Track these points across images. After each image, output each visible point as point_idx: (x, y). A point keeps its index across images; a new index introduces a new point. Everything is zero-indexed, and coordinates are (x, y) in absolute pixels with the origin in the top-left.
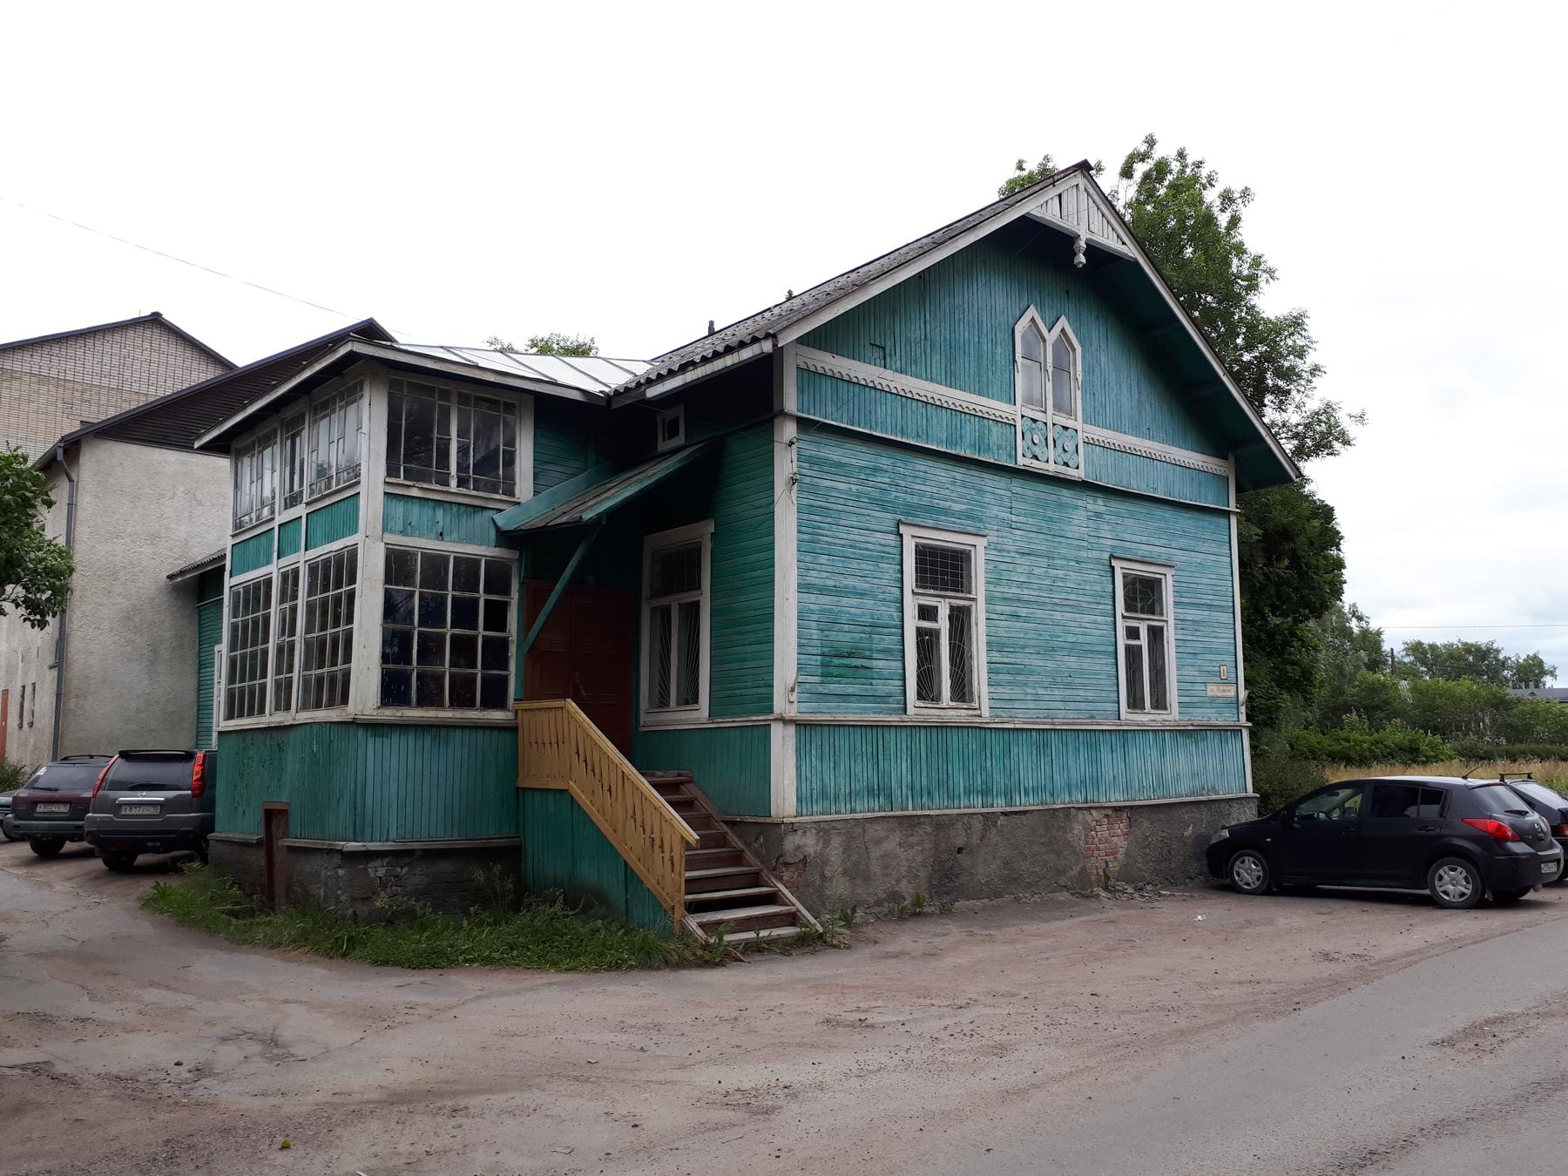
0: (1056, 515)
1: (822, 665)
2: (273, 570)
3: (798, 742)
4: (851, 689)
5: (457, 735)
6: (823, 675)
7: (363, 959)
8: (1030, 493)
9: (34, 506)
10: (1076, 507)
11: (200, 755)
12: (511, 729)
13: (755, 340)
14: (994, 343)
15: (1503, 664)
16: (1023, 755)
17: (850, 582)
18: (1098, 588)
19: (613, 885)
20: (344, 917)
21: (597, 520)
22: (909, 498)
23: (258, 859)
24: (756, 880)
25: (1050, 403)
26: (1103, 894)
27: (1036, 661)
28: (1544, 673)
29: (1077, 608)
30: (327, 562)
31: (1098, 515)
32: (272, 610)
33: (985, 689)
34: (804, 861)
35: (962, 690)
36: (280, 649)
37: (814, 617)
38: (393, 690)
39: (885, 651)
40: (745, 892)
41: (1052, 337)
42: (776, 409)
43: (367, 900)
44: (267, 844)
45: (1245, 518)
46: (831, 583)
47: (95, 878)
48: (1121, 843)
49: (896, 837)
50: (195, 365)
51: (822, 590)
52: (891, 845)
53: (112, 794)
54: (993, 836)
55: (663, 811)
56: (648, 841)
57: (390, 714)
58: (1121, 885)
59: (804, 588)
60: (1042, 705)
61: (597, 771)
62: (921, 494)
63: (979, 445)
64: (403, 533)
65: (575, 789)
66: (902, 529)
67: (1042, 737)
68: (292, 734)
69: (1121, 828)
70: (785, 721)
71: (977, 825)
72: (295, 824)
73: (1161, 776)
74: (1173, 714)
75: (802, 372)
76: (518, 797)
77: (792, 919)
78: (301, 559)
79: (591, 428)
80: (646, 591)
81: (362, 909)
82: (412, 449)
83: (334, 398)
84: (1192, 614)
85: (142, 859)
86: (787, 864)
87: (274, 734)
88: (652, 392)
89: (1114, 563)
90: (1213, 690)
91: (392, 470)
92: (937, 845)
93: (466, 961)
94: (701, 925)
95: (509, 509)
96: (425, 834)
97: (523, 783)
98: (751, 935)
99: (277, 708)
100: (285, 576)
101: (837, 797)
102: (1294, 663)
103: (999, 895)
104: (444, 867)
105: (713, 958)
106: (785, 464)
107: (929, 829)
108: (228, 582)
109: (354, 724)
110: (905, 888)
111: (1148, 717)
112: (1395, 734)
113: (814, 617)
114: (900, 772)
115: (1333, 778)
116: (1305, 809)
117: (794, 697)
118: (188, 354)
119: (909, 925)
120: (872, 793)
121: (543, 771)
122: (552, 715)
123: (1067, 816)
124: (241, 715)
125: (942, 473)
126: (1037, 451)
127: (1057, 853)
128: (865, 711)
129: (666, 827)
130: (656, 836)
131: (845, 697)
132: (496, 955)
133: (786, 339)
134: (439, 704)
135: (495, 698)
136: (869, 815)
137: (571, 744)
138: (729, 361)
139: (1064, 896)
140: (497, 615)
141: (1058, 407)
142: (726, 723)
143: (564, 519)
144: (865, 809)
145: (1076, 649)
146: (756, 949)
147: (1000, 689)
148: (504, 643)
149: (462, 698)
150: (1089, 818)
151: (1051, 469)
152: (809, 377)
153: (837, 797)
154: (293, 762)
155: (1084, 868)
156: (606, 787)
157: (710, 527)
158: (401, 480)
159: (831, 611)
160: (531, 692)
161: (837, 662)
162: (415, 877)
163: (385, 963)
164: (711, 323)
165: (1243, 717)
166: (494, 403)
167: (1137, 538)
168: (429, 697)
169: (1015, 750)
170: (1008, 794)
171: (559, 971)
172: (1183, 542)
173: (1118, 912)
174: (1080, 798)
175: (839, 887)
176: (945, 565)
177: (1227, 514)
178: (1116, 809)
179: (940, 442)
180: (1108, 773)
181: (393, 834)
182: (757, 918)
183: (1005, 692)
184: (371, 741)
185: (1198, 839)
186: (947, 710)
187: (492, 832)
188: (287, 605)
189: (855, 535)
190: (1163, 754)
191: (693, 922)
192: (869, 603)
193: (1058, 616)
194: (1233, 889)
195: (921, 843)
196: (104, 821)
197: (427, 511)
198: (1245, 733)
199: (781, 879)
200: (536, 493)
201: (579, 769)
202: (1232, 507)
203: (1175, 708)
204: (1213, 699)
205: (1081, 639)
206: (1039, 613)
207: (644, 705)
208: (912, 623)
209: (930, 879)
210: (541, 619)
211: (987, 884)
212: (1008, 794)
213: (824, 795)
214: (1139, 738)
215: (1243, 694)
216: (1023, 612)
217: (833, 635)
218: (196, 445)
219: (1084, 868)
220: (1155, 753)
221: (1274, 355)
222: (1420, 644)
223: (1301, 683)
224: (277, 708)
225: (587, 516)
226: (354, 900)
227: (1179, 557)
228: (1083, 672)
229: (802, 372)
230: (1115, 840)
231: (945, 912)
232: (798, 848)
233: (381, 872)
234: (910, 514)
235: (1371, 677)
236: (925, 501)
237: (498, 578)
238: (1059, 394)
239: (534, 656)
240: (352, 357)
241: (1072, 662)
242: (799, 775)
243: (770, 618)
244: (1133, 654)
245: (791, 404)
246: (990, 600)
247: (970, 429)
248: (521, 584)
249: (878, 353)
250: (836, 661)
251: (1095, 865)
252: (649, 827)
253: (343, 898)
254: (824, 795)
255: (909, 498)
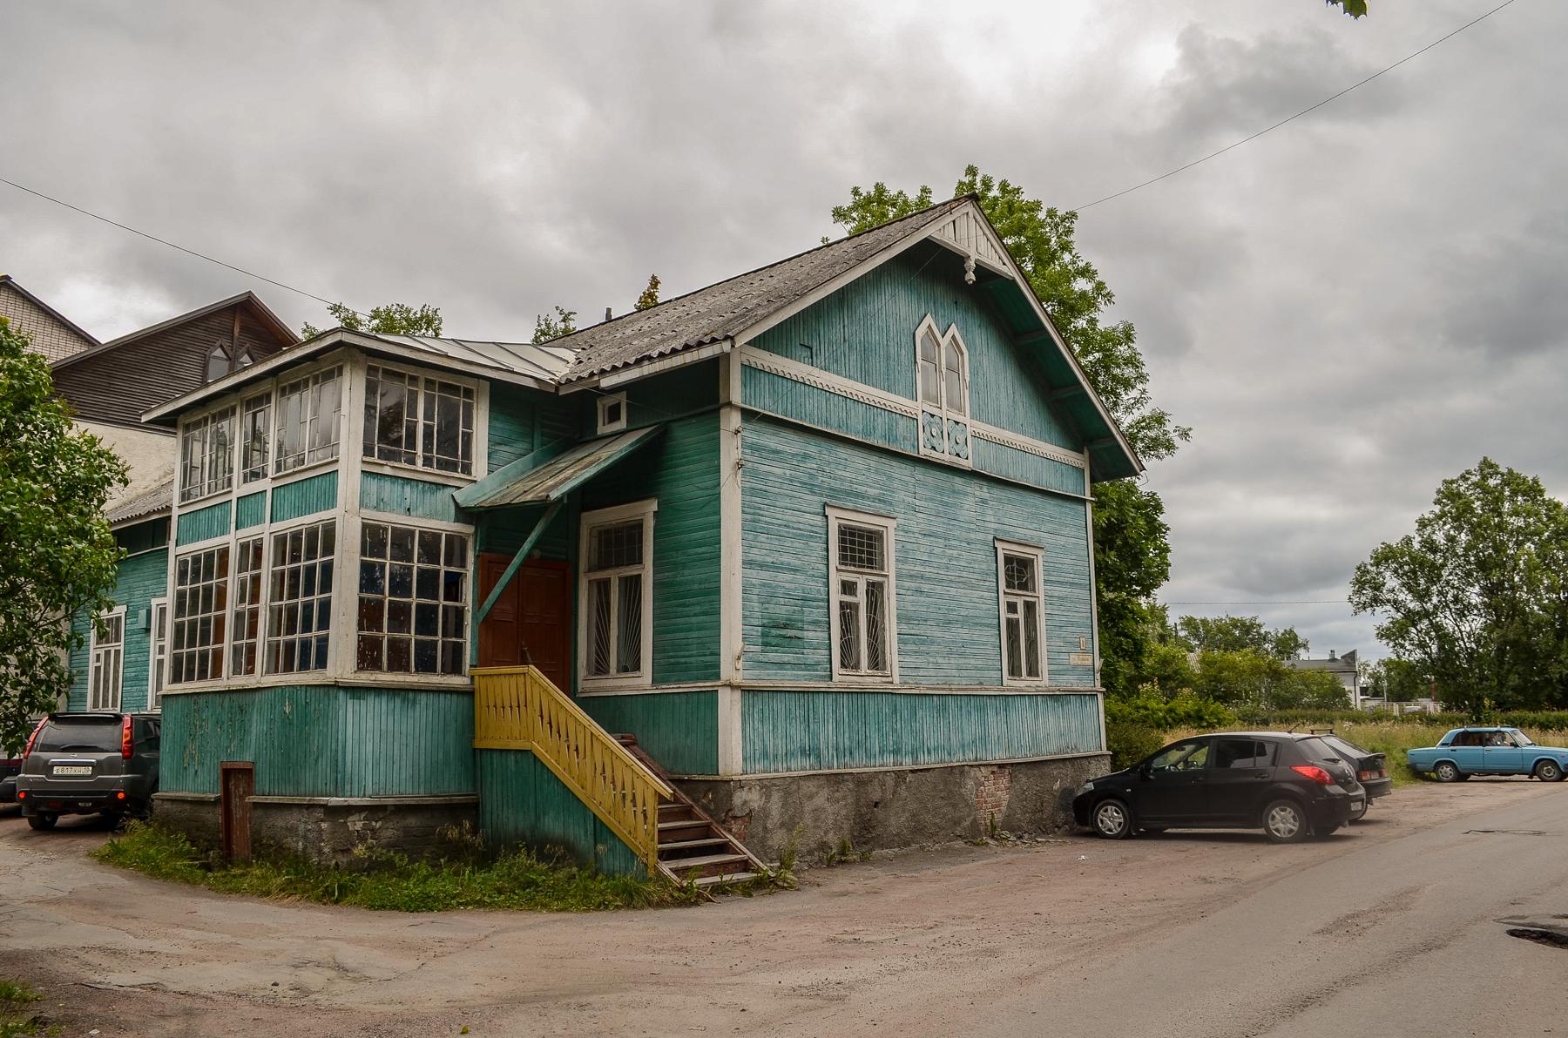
0: (951, 500)
1: (764, 635)
2: (232, 540)
3: (743, 706)
4: (787, 658)
5: (423, 698)
6: (765, 644)
7: (358, 904)
8: (929, 480)
9: (110, 485)
10: (966, 494)
11: (127, 719)
12: (469, 694)
13: (714, 341)
14: (899, 346)
15: (1265, 638)
16: (925, 716)
17: (785, 559)
18: (984, 566)
19: (581, 836)
20: (328, 867)
21: (560, 500)
22: (832, 482)
23: (215, 817)
24: (707, 831)
25: (944, 400)
26: (991, 842)
27: (936, 633)
28: (1298, 646)
29: (967, 584)
30: (296, 537)
31: (984, 501)
32: (230, 579)
33: (896, 658)
34: (749, 815)
35: (877, 661)
36: (239, 616)
37: (756, 591)
38: (368, 656)
39: (814, 623)
40: (707, 843)
41: (945, 342)
42: (722, 401)
43: (347, 851)
44: (225, 801)
45: (1100, 506)
46: (769, 560)
47: (23, 837)
48: (1004, 797)
49: (825, 793)
50: (40, 329)
51: (762, 566)
52: (820, 800)
53: (45, 755)
54: (903, 792)
55: (635, 768)
56: (619, 797)
57: (367, 678)
58: (1006, 833)
59: (748, 564)
60: (941, 673)
61: (563, 732)
62: (842, 479)
63: (890, 434)
64: (377, 508)
65: (539, 750)
66: (828, 511)
67: (941, 700)
68: (258, 696)
69: (1004, 782)
70: (732, 687)
71: (890, 782)
72: (263, 780)
73: (1034, 737)
74: (1044, 681)
75: (747, 368)
76: (475, 759)
77: (745, 866)
78: (265, 531)
79: (546, 416)
80: (583, 566)
81: (343, 859)
82: (387, 434)
83: (306, 382)
84: (1059, 591)
85: (62, 820)
86: (735, 818)
87: (234, 697)
88: (605, 383)
89: (997, 544)
90: (1074, 659)
91: (368, 451)
92: (858, 800)
93: (460, 904)
94: (675, 871)
95: (467, 487)
96: (396, 789)
97: (479, 744)
98: (717, 879)
99: (236, 671)
100: (244, 547)
101: (775, 756)
102: (1127, 636)
103: (907, 844)
104: (412, 821)
105: (688, 899)
106: (730, 451)
107: (851, 786)
108: (173, 550)
109: (336, 686)
110: (833, 839)
111: (1024, 683)
112: (1186, 701)
113: (756, 591)
114: (827, 734)
115: (1168, 740)
116: (1158, 763)
117: (739, 666)
118: (34, 316)
119: (839, 871)
120: (803, 752)
121: (501, 732)
122: (513, 680)
123: (962, 773)
124: (190, 678)
125: (859, 460)
126: (934, 441)
127: (954, 806)
128: (797, 678)
129: (638, 783)
130: (628, 791)
131: (781, 665)
132: (486, 899)
133: (741, 341)
134: (406, 669)
135: (455, 667)
136: (802, 773)
137: (531, 711)
138: (689, 358)
139: (959, 844)
140: (454, 583)
141: (950, 404)
142: (672, 688)
143: (529, 497)
144: (800, 766)
145: (966, 622)
146: (720, 890)
147: (908, 659)
148: (460, 612)
149: (426, 665)
150: (979, 774)
151: (946, 458)
152: (750, 371)
153: (775, 756)
154: (257, 726)
155: (975, 820)
156: (573, 747)
157: (653, 506)
158: (375, 459)
159: (769, 586)
160: (485, 658)
161: (776, 633)
162: (389, 830)
163: (383, 907)
164: (609, 310)
165: (1098, 683)
166: (454, 389)
167: (1013, 522)
168: (398, 662)
169: (919, 714)
170: (914, 753)
171: (552, 911)
172: (1049, 527)
173: (1008, 857)
174: (972, 757)
175: (778, 839)
176: (861, 544)
177: (1083, 502)
178: (1001, 766)
179: (857, 433)
180: (994, 732)
181: (369, 792)
182: (715, 865)
183: (910, 660)
184: (350, 702)
185: (1066, 792)
186: (873, 681)
187: (452, 787)
188: (247, 575)
189: (789, 516)
190: (1036, 717)
191: (666, 868)
192: (800, 577)
193: (953, 591)
194: (1097, 834)
195: (844, 798)
196: (36, 782)
197: (397, 488)
198: (1100, 697)
199: (730, 831)
200: (490, 472)
201: (542, 731)
202: (1088, 496)
203: (1046, 675)
204: (1075, 666)
205: (971, 613)
206: (939, 589)
207: (582, 672)
208: (836, 597)
209: (852, 830)
210: (497, 590)
211: (898, 835)
212: (914, 753)
213: (765, 755)
214: (1018, 701)
215: (1098, 664)
216: (926, 587)
217: (772, 608)
218: (144, 419)
219: (975, 820)
220: (1030, 715)
221: (1115, 361)
222: (1192, 618)
223: (1136, 651)
224: (236, 671)
225: (554, 495)
226: (335, 851)
227: (1046, 539)
228: (973, 643)
229: (747, 368)
230: (996, 796)
231: (864, 860)
232: (745, 802)
233: (359, 826)
234: (833, 498)
235: (1162, 650)
236: (846, 486)
237: (456, 547)
238: (954, 389)
239: (488, 625)
240: (340, 344)
241: (964, 633)
242: (744, 737)
243: (717, 591)
244: (1012, 626)
245: (736, 396)
246: (899, 577)
247: (881, 421)
248: (477, 557)
249: (807, 353)
250: (774, 632)
251: (984, 816)
252: (622, 785)
253: (326, 850)
254: (765, 755)
255: (832, 482)
